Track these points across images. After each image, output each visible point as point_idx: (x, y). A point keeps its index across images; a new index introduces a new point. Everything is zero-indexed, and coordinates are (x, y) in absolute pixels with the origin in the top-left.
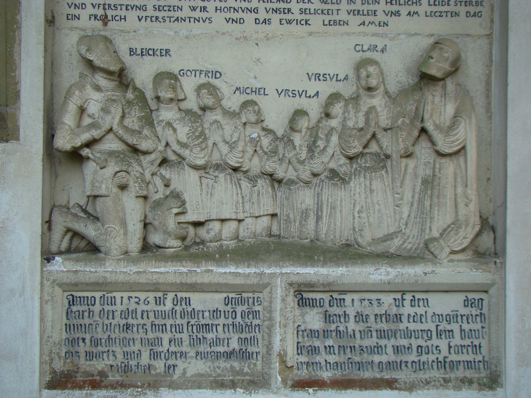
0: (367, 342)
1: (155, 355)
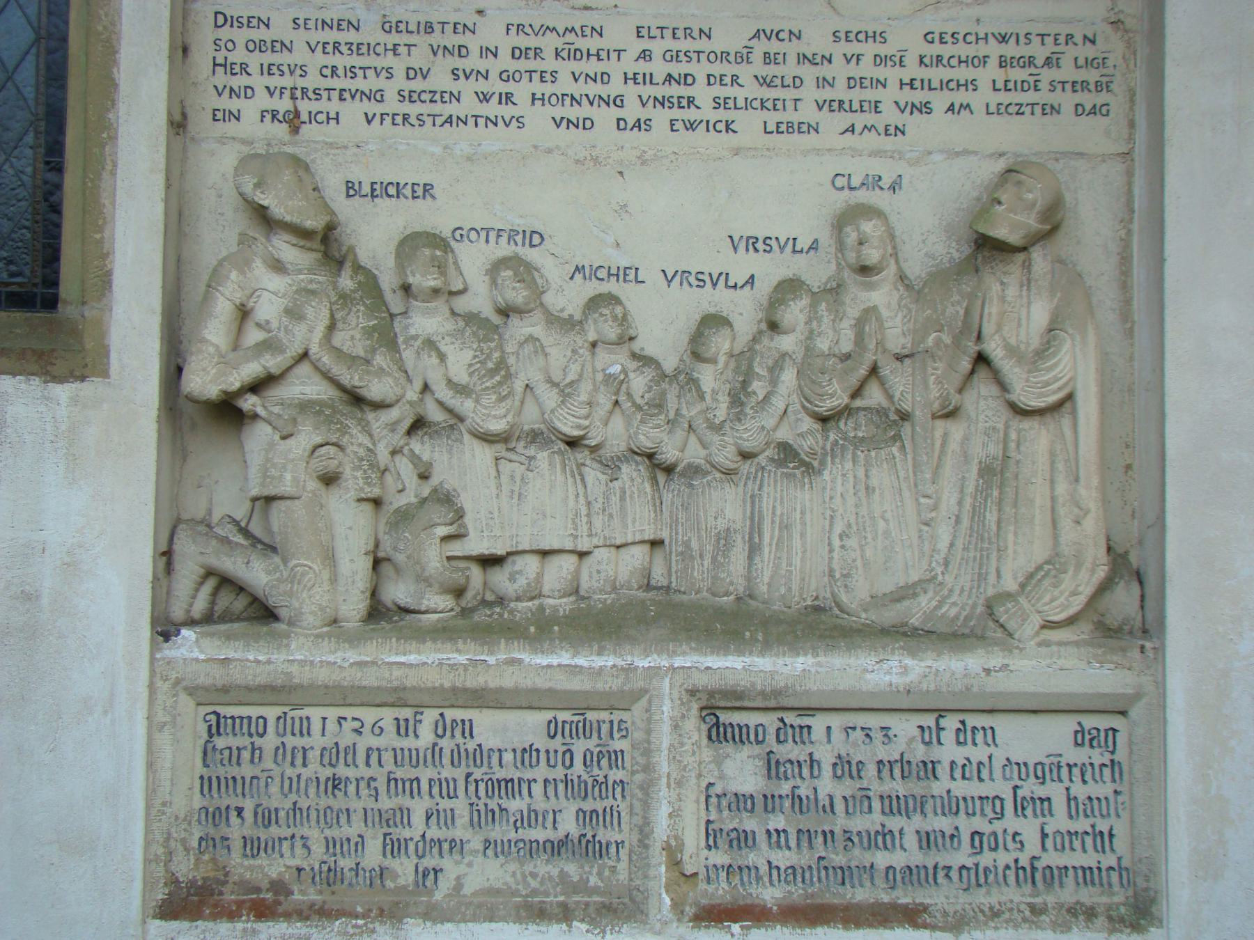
0: (859, 823)
1: (394, 847)
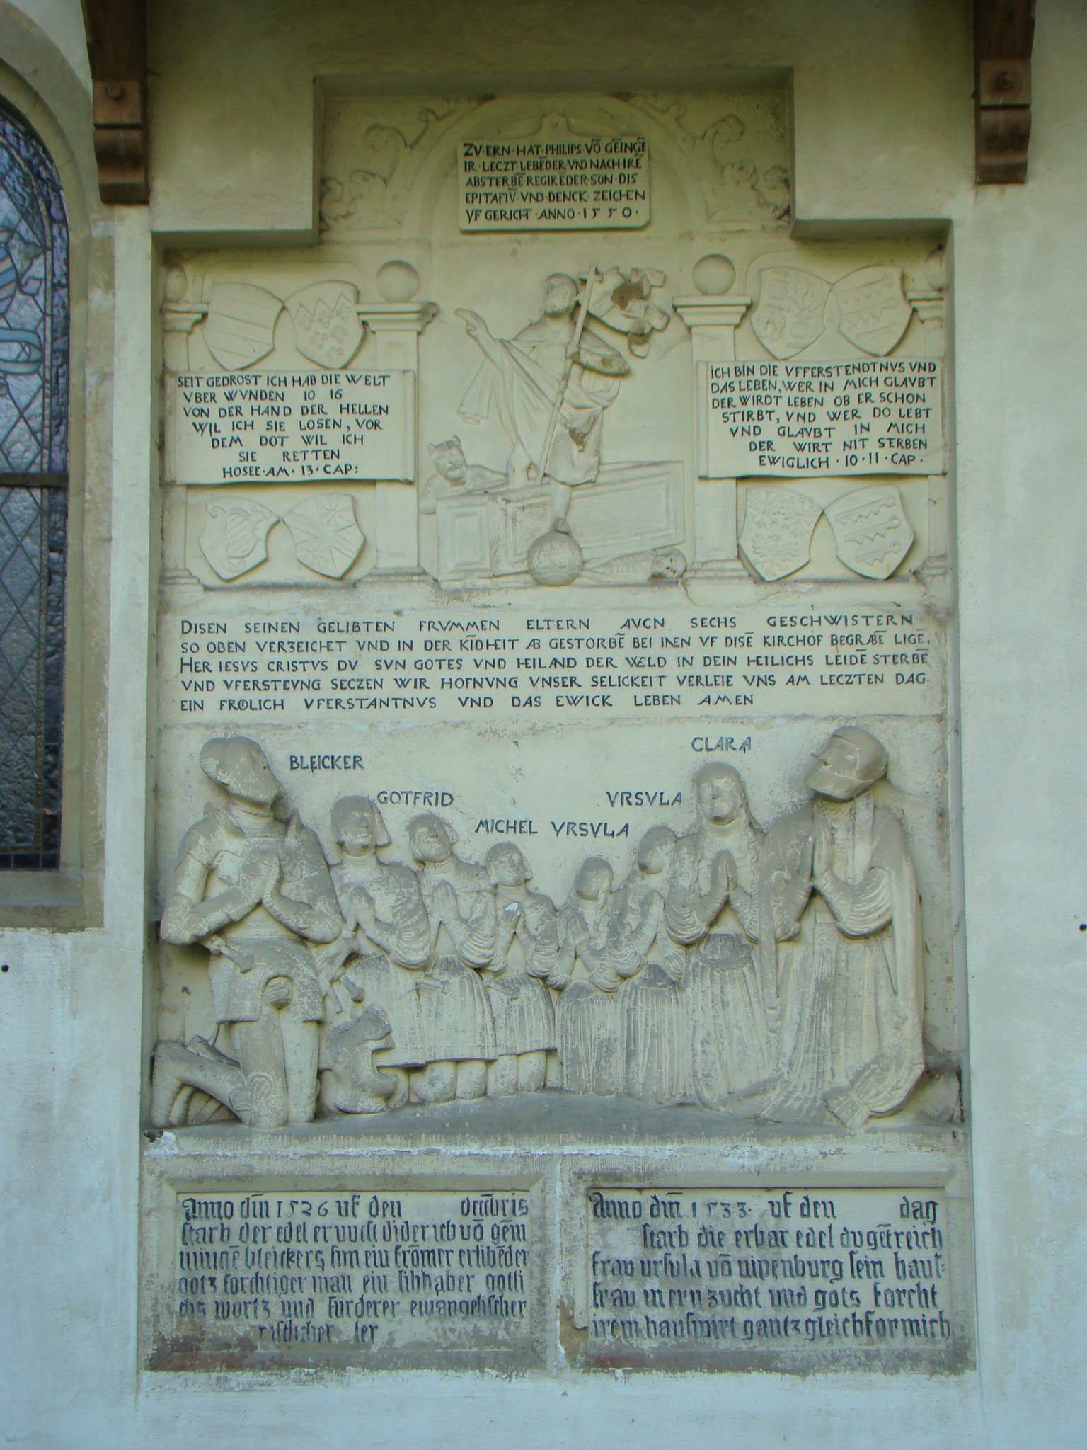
0: (721, 1284)
1: (338, 1308)
